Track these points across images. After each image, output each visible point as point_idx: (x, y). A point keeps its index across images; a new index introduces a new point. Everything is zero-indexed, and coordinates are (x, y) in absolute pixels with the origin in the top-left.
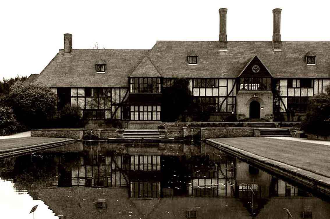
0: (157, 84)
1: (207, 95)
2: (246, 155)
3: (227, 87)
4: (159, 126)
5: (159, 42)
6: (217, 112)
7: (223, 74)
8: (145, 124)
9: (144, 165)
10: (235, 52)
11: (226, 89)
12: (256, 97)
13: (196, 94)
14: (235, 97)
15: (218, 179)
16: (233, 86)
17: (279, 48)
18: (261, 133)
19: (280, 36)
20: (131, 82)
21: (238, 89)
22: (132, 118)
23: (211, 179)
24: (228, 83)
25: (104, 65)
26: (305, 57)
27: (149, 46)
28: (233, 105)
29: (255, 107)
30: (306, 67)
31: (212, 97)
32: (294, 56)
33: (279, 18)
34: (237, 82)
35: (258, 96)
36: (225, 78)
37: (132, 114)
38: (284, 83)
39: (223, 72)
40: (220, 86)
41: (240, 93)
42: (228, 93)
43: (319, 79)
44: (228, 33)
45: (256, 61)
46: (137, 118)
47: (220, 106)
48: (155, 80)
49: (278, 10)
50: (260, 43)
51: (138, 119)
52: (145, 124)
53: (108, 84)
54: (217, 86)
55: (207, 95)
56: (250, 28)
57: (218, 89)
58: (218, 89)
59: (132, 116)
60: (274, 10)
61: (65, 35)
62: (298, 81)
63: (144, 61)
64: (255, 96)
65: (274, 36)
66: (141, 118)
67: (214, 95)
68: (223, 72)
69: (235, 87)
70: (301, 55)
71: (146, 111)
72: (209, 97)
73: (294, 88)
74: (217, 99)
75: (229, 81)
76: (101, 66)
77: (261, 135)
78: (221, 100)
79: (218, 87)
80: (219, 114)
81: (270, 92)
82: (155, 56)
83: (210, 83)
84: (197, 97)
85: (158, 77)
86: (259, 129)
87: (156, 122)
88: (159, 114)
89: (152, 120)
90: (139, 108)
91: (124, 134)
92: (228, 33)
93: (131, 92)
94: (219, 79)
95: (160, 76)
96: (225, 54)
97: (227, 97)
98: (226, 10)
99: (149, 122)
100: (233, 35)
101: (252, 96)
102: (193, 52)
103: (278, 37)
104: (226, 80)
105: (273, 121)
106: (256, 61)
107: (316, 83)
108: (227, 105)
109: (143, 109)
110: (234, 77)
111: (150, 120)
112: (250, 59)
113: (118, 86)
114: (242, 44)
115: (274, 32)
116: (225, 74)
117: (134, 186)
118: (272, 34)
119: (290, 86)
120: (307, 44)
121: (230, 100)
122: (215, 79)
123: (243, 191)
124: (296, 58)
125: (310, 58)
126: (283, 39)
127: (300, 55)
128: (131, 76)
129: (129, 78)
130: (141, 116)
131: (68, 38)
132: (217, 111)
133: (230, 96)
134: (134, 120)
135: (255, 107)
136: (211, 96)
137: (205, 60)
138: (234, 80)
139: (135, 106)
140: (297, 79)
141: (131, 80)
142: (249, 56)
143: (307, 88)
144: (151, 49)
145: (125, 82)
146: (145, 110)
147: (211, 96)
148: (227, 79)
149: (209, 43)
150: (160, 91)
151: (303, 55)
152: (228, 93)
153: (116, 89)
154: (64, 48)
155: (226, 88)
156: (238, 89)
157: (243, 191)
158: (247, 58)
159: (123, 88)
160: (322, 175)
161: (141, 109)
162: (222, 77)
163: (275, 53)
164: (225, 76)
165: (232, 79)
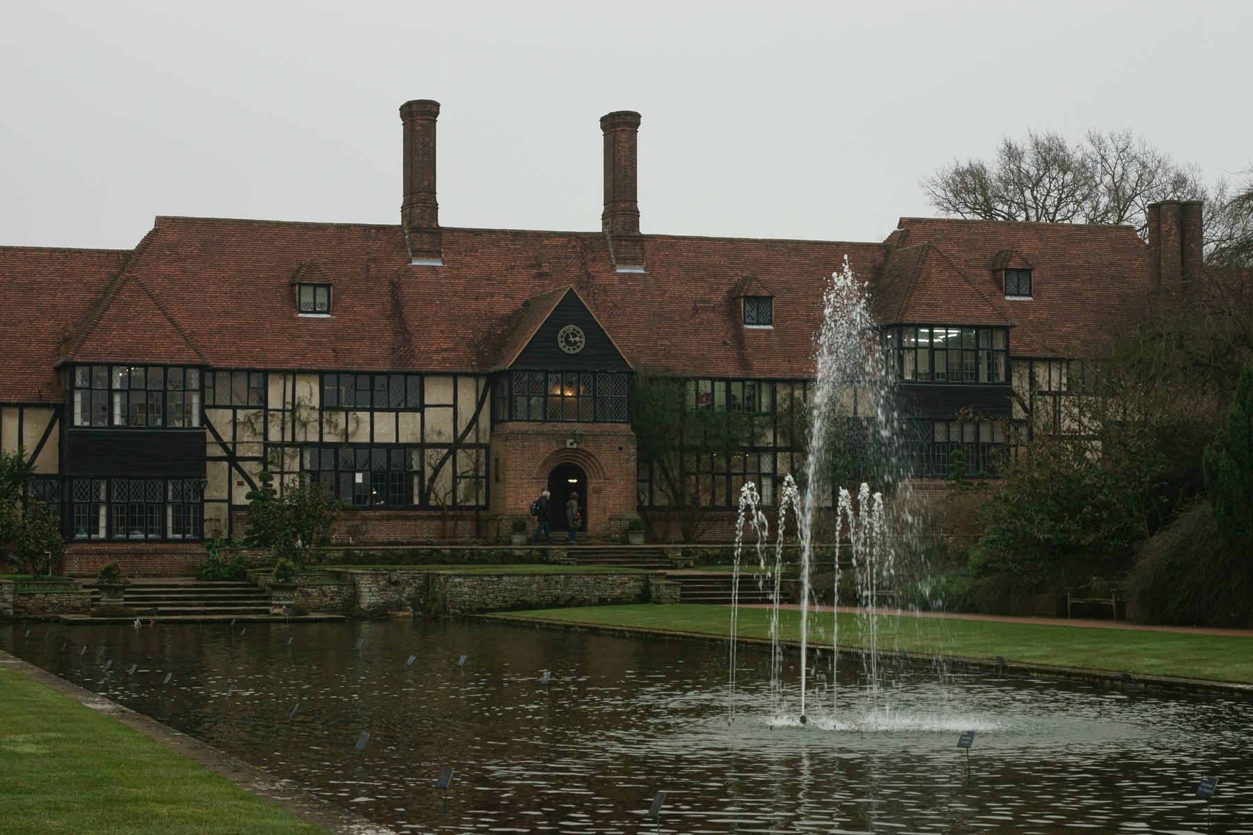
5: (163, 223)
6: (416, 508)
8: (138, 554)
9: (266, 438)
12: (575, 446)
14: (487, 447)
16: (479, 405)
17: (634, 261)
18: (682, 589)
26: (733, 299)
27: (128, 239)
28: (476, 477)
30: (739, 336)
31: (397, 445)
34: (497, 388)
35: (582, 446)
41: (512, 433)
42: (460, 432)
43: (283, 373)
44: (644, 202)
45: (571, 309)
52: (138, 554)
55: (376, 440)
57: (418, 415)
58: (418, 415)
60: (409, 104)
64: (568, 446)
65: (407, 208)
70: (718, 289)
74: (415, 456)
75: (460, 381)
77: (682, 595)
78: (433, 456)
79: (421, 408)
80: (424, 514)
81: (624, 428)
82: (159, 280)
86: (669, 572)
87: (180, 546)
91: (126, 599)
95: (198, 361)
98: (434, 110)
100: (658, 216)
101: (558, 444)
104: (451, 381)
105: (646, 543)
108: (455, 477)
113: (13, 400)
116: (446, 355)
121: (464, 461)
124: (701, 302)
132: (416, 502)
135: (566, 483)
136: (394, 441)
137: (361, 299)
138: (482, 383)
144: (130, 242)
147: (394, 441)
148: (455, 376)
152: (460, 432)
153: (271, 377)
165: (475, 376)
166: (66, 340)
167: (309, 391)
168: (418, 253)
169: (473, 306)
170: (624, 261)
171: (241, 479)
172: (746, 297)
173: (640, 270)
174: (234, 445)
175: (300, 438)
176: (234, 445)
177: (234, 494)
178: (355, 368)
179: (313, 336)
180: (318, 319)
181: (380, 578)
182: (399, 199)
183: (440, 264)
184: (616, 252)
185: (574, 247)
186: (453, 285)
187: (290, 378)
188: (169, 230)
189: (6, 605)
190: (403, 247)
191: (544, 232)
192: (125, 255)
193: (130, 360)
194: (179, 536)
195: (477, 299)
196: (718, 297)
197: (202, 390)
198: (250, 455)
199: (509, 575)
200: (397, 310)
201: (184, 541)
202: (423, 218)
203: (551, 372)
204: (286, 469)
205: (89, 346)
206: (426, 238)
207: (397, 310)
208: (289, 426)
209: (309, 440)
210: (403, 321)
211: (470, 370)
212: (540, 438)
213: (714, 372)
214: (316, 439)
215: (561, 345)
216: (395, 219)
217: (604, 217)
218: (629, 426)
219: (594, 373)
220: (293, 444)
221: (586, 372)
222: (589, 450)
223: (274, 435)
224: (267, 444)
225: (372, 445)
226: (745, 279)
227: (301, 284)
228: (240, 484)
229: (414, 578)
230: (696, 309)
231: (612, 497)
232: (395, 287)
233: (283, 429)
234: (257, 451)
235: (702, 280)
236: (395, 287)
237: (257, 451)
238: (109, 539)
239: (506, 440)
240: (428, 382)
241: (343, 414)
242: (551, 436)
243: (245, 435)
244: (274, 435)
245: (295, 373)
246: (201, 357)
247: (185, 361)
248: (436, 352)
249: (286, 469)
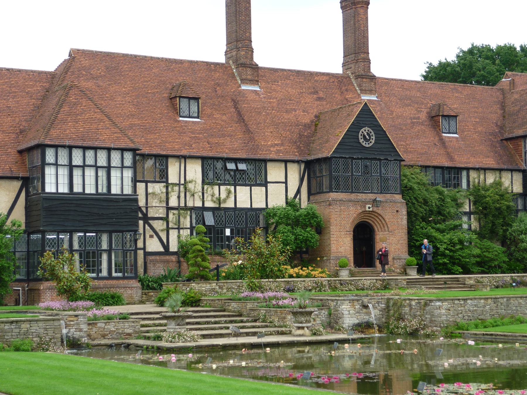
3: (286, 183)
4: (388, 264)
5: (76, 55)
9: (167, 203)
12: (371, 210)
16: (302, 180)
17: (371, 92)
23: (83, 193)
29: (364, 235)
30: (442, 141)
31: (251, 209)
32: (409, 112)
34: (313, 169)
40: (269, 180)
50: (325, 78)
58: (264, 189)
64: (367, 209)
79: (265, 184)
81: (398, 197)
83: (253, 172)
87: (121, 282)
92: (373, 55)
95: (132, 146)
102: (177, 85)
104: (283, 165)
109: (82, 160)
124: (414, 118)
133: (146, 225)
136: (249, 206)
143: (57, 193)
146: (90, 161)
147: (249, 206)
148: (286, 162)
153: (187, 160)
162: (272, 156)
164: (281, 156)
165: (298, 162)
166: (21, 132)
167: (194, 171)
168: (244, 81)
169: (286, 117)
170: (364, 91)
171: (152, 233)
172: (443, 116)
173: (256, 88)
174: (147, 208)
175: (190, 204)
176: (147, 208)
177: (147, 244)
178: (225, 156)
179: (193, 133)
180: (193, 122)
181: (356, 303)
182: (222, 46)
183: (258, 89)
184: (360, 86)
185: (334, 82)
186: (270, 103)
187: (183, 160)
188: (80, 62)
189: (82, 334)
191: (314, 72)
192: (51, 76)
193: (85, 144)
194: (120, 275)
195: (286, 112)
196: (423, 116)
197: (134, 167)
198: (157, 215)
199: (471, 299)
200: (240, 117)
201: (124, 278)
202: (246, 58)
203: (355, 159)
204: (181, 226)
205: (54, 133)
206: (249, 71)
207: (240, 117)
208: (182, 195)
209: (196, 205)
210: (246, 125)
211: (296, 158)
212: (350, 204)
214: (200, 205)
215: (361, 141)
216: (337, 69)
217: (344, 65)
218: (401, 196)
219: (380, 160)
220: (186, 208)
221: (375, 159)
222: (379, 212)
223: (173, 202)
224: (169, 209)
227: (180, 97)
228: (151, 236)
229: (378, 303)
231: (392, 239)
232: (235, 103)
233: (179, 197)
234: (161, 213)
235: (410, 105)
236: (235, 103)
237: (161, 213)
238: (110, 277)
239: (330, 205)
240: (269, 165)
241: (217, 187)
242: (355, 202)
243: (154, 202)
244: (173, 202)
246: (133, 142)
247: (123, 146)
248: (272, 146)
249: (181, 226)
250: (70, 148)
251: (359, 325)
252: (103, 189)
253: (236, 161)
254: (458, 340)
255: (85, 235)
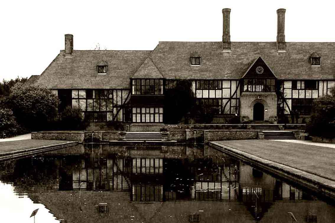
0: (160, 85)
1: (210, 97)
2: (249, 157)
3: (231, 88)
4: (161, 129)
5: (161, 43)
6: (220, 114)
7: (226, 75)
8: (148, 126)
9: (146, 168)
10: (239, 53)
11: (230, 91)
12: (260, 98)
13: (199, 96)
14: (239, 99)
15: (221, 182)
16: (237, 88)
17: (283, 49)
19: (284, 36)
20: (133, 83)
21: (242, 90)
22: (134, 121)
24: (232, 85)
25: (106, 66)
26: (310, 58)
27: (151, 47)
28: (236, 106)
29: (259, 109)
30: (310, 68)
31: (215, 98)
33: (284, 18)
34: (241, 83)
35: (262, 98)
36: (228, 80)
37: (134, 116)
38: (288, 85)
39: (226, 73)
40: (223, 87)
41: (244, 95)
42: (232, 95)
43: (323, 81)
44: (231, 34)
45: (260, 62)
46: (139, 121)
47: (223, 108)
48: (157, 81)
49: (283, 10)
50: (264, 44)
51: (140, 121)
52: (148, 126)
53: (110, 86)
54: (220, 88)
55: (210, 97)
56: (254, 29)
57: (221, 91)
58: (221, 91)
59: (134, 118)
60: (278, 10)
61: (66, 36)
62: (303, 83)
63: (146, 62)
64: (258, 98)
65: (278, 37)
66: (143, 121)
67: (217, 97)
68: (226, 73)
69: (239, 88)
70: (306, 56)
71: (148, 113)
72: (213, 99)
73: (299, 90)
74: (220, 101)
75: (232, 82)
76: (103, 67)
77: (265, 137)
78: (225, 101)
79: (222, 89)
80: (222, 116)
82: (157, 57)
83: (213, 84)
84: (200, 99)
85: (161, 79)
86: (263, 131)
87: (158, 124)
88: (161, 116)
89: (154, 122)
90: (141, 110)
91: (126, 137)
92: (231, 34)
93: (133, 93)
94: (222, 80)
96: (228, 55)
97: (230, 99)
98: (230, 10)
99: (151, 124)
101: (256, 97)
102: (196, 53)
103: (282, 37)
104: (229, 82)
105: (277, 124)
106: (260, 62)
107: (321, 84)
108: (231, 107)
109: (145, 111)
110: (237, 78)
111: (152, 123)
112: (254, 60)
113: (120, 88)
114: (246, 45)
115: (278, 33)
116: (228, 75)
117: (136, 189)
118: (276, 35)
119: (294, 87)
120: (312, 45)
121: (234, 102)
122: (218, 80)
123: (246, 194)
124: (300, 59)
125: (315, 60)
126: (287, 40)
127: (304, 56)
128: (133, 78)
129: (131, 80)
130: (143, 118)
131: (69, 39)
132: (220, 113)
133: (233, 97)
134: (136, 122)
135: (259, 109)
136: (214, 97)
137: (208, 61)
138: (238, 82)
139: (137, 107)
140: (301, 81)
141: (133, 81)
142: (253, 57)
143: (312, 90)
144: (153, 49)
145: (127, 83)
146: (148, 112)
147: (214, 97)
148: (231, 80)
149: (212, 44)
150: (162, 93)
151: (308, 56)
152: (232, 95)
153: (118, 91)
154: (65, 49)
155: (230, 89)
156: (242, 90)
157: (246, 194)
158: (251, 59)
159: (125, 89)
160: (327, 178)
161: (143, 111)
162: (225, 78)
163: (279, 54)
164: (229, 78)
165: (236, 80)
190: (221, 47)
213: (301, 78)
225: (209, 99)
226: (314, 53)
230: (299, 61)
245: (78, 90)
250: (154, 122)
251: (312, 166)
252: (143, 161)
253: (78, 90)
254: (268, 144)
255: (285, 125)
